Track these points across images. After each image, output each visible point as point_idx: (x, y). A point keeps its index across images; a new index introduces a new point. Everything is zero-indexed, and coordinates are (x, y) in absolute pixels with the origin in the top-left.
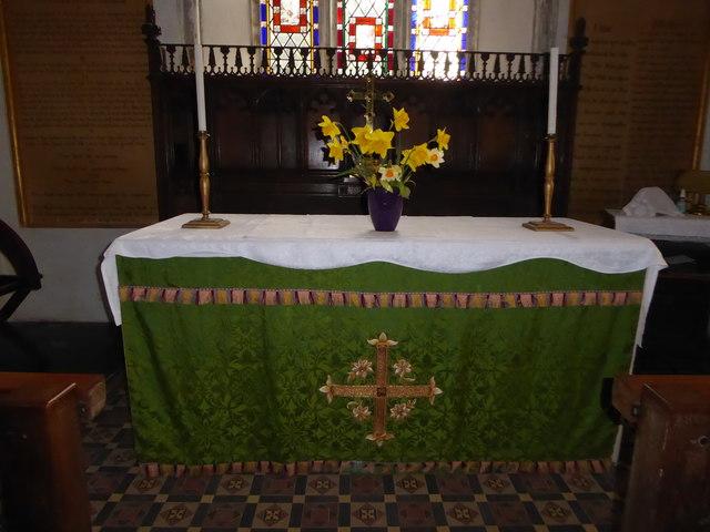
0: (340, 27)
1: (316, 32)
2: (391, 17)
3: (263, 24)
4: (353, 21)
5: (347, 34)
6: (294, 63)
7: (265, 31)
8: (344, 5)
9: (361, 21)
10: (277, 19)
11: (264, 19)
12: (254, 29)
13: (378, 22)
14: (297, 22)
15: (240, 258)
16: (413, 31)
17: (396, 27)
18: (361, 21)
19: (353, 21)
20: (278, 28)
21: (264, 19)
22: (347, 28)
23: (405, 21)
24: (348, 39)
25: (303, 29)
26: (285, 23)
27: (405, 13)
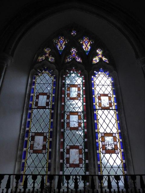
0: (62, 150)
1: (50, 142)
2: (86, 145)
3: (25, 149)
4: (68, 147)
5: (65, 154)
6: (27, 186)
7: (25, 152)
8: (64, 140)
9: (44, 108)
10: (32, 147)
11: (26, 147)
12: (19, 152)
13: (81, 147)
14: (41, 148)
15: (4, 178)
16: (98, 151)
17: (89, 150)
18: (44, 108)
19: (81, 165)
20: (32, 151)
21: (26, 147)
22: (65, 151)
23: (93, 147)
24: (66, 156)
25: (44, 151)
26: (36, 149)
27: (93, 144)
